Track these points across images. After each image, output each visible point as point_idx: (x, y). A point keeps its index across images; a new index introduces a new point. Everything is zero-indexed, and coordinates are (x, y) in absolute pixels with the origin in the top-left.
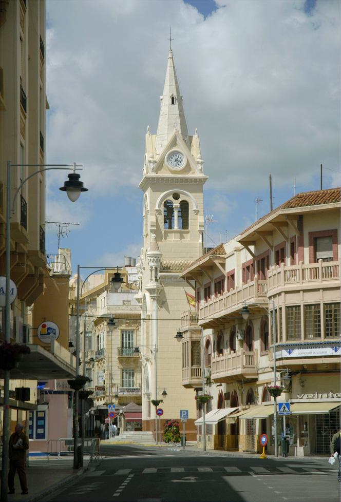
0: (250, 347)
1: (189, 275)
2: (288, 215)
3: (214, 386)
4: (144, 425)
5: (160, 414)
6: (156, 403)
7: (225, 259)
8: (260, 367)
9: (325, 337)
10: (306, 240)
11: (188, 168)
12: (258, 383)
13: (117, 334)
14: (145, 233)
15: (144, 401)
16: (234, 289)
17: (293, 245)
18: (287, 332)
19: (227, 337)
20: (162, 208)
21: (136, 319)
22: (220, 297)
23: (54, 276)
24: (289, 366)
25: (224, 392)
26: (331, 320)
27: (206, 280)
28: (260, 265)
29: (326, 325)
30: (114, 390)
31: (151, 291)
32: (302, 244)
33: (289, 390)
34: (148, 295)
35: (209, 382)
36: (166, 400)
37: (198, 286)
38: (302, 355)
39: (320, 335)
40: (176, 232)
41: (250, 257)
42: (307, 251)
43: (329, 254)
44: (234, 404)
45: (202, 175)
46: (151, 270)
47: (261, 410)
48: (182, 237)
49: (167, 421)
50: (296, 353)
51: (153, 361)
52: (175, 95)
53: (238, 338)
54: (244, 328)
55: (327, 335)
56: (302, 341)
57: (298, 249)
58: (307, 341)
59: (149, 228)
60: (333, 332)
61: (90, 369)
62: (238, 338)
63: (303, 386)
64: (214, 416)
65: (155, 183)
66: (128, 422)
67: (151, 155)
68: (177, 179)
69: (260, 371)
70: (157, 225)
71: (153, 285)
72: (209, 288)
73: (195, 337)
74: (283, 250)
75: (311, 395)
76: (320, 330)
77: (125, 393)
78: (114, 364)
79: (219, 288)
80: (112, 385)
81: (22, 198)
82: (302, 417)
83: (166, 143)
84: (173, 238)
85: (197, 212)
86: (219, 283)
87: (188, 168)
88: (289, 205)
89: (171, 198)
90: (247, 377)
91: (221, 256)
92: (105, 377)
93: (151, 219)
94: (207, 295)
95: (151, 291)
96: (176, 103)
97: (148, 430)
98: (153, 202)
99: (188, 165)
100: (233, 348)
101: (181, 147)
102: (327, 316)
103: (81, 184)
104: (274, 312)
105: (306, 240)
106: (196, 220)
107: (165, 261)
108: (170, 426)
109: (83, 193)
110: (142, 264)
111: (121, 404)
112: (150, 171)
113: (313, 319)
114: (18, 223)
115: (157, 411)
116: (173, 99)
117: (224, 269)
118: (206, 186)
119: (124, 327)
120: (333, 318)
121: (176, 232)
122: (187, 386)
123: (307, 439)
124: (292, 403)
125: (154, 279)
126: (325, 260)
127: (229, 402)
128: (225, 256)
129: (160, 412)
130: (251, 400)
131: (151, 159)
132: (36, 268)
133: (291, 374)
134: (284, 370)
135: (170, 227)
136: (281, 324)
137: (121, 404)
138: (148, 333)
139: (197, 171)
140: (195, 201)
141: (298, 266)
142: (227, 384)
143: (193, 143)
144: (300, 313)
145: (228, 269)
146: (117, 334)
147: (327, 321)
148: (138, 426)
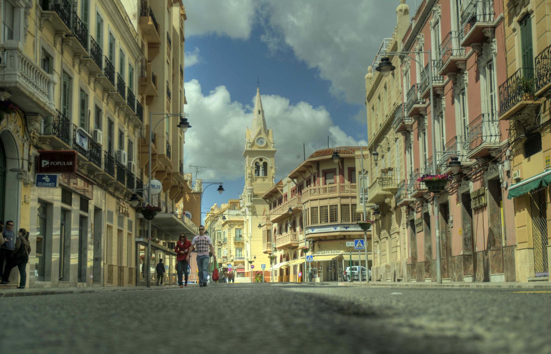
0: (295, 230)
1: (266, 197)
2: (312, 162)
3: (278, 252)
4: (246, 274)
5: (253, 268)
6: (251, 262)
7: (283, 187)
8: (300, 240)
9: (330, 222)
10: (321, 174)
11: (267, 146)
12: (298, 248)
13: (233, 231)
14: (246, 179)
15: (246, 263)
16: (287, 201)
17: (314, 177)
18: (312, 220)
19: (284, 227)
20: (254, 166)
21: (241, 223)
22: (280, 206)
23: (193, 193)
24: (312, 237)
25: (283, 254)
26: (333, 214)
27: (274, 199)
28: (299, 189)
29: (331, 216)
30: (232, 258)
31: (248, 207)
32: (319, 176)
33: (313, 250)
34: (247, 209)
35: (276, 250)
36: (256, 260)
37: (270, 202)
38: (318, 232)
39: (327, 221)
40: (261, 178)
41: (294, 185)
42: (321, 179)
43: (332, 181)
44: (288, 260)
45: (274, 149)
46: (249, 197)
47: (300, 261)
48: (264, 180)
49: (256, 272)
50: (316, 230)
51: (250, 242)
52: (260, 109)
53: (289, 226)
54: (292, 221)
55: (331, 221)
56: (319, 224)
57: (317, 179)
58: (321, 225)
59: (248, 176)
60: (334, 219)
61: (220, 249)
62: (289, 226)
63: (319, 248)
64: (279, 265)
65: (250, 153)
66: (238, 273)
67: (248, 139)
68: (261, 151)
69: (300, 242)
70: (251, 174)
71: (249, 204)
72: (276, 203)
73: (269, 228)
74: (310, 180)
75: (323, 252)
76: (328, 219)
77: (238, 260)
78: (232, 245)
79: (280, 202)
80: (231, 256)
81: (168, 143)
82: (319, 262)
83: (256, 133)
84: (259, 181)
85: (272, 168)
86: (280, 200)
87: (267, 146)
88: (312, 156)
89: (258, 161)
90: (293, 245)
91: (281, 186)
92: (227, 252)
93: (249, 171)
94: (275, 206)
95: (248, 207)
96: (261, 113)
97: (248, 276)
98: (249, 163)
99: (267, 144)
100: (286, 231)
101: (263, 135)
102: (331, 212)
103: (188, 123)
104: (305, 211)
105: (321, 174)
106: (271, 172)
107: (256, 192)
108: (258, 274)
109: (189, 129)
110: (244, 194)
111: (235, 265)
112: (248, 147)
113: (324, 213)
114: (164, 155)
115: (251, 266)
116: (259, 111)
117: (283, 192)
118: (276, 154)
119: (236, 227)
120: (334, 213)
121: (261, 178)
122: (265, 253)
123: (322, 274)
124: (314, 256)
125: (250, 201)
126: (330, 184)
127: (285, 259)
128: (283, 186)
129: (253, 267)
130: (295, 257)
131: (249, 142)
132: (179, 183)
133: (314, 242)
134: (310, 240)
135: (258, 175)
136: (308, 216)
137: (235, 265)
138: (247, 228)
139: (272, 147)
140: (270, 162)
141: (317, 187)
142: (284, 250)
143: (269, 133)
144: (318, 211)
145: (284, 192)
146: (233, 231)
147: (331, 214)
148: (243, 274)
